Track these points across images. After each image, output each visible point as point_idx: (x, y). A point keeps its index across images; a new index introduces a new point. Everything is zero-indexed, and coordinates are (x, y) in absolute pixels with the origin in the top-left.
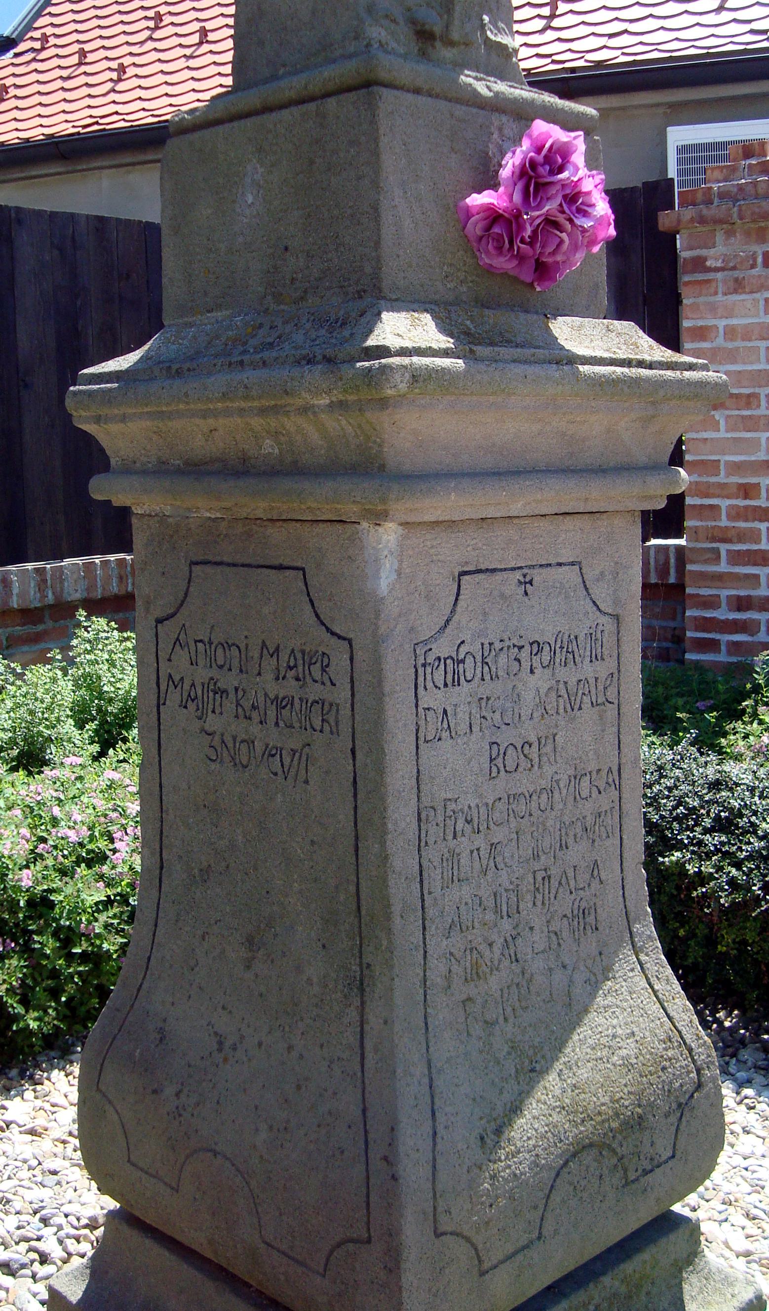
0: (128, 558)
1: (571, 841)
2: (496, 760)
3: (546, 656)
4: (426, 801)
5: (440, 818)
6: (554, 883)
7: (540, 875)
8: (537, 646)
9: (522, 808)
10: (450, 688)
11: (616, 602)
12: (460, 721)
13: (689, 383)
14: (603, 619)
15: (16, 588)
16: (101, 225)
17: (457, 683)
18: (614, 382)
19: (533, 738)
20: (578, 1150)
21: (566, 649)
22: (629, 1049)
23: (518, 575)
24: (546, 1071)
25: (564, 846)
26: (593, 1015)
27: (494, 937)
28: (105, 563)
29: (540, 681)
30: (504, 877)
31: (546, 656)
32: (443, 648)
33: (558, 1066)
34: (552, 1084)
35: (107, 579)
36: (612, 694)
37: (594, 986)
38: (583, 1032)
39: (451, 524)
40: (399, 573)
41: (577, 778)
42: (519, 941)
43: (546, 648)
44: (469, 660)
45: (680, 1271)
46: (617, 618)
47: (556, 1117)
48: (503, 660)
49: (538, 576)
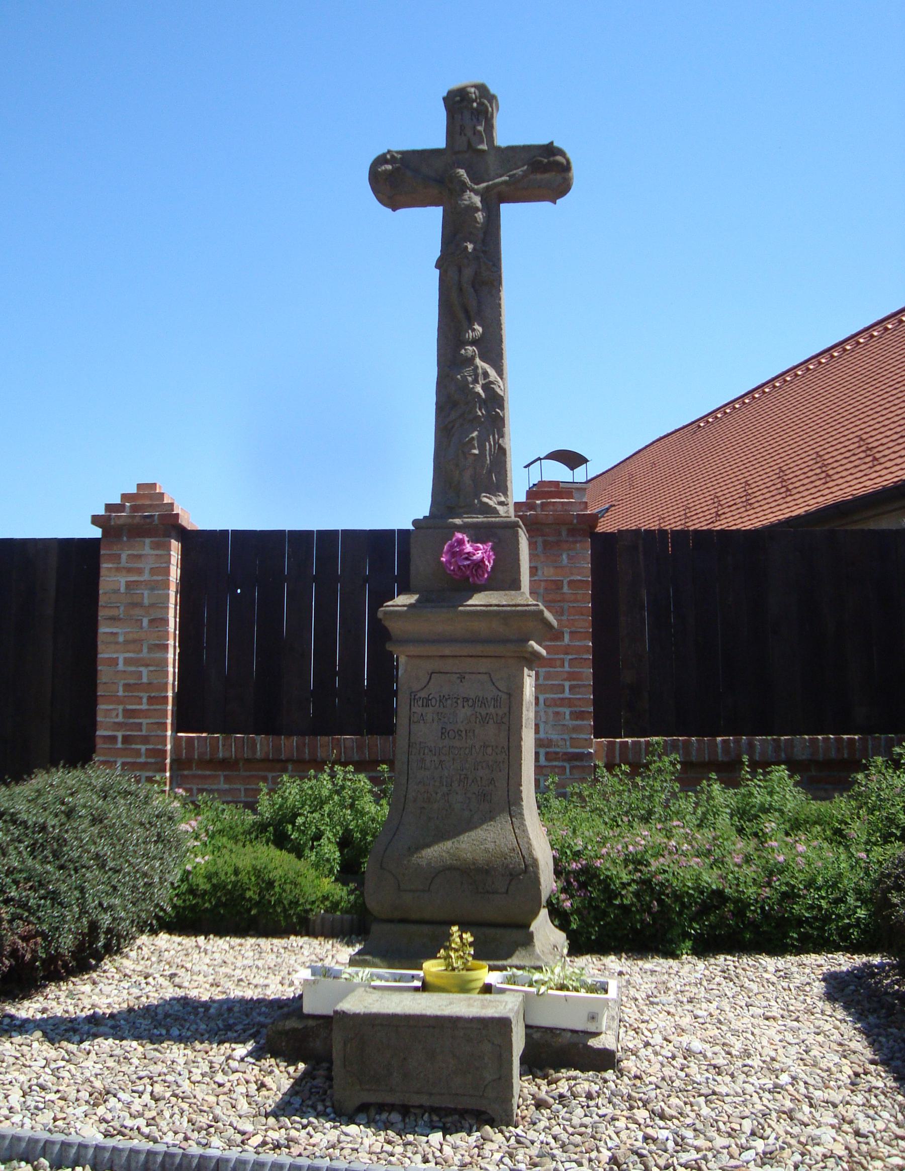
0: (856, 737)
1: (480, 767)
2: (444, 733)
3: (470, 703)
4: (412, 740)
6: (470, 781)
8: (466, 699)
13: (518, 611)
14: (500, 694)
17: (428, 706)
18: (482, 611)
19: (462, 729)
20: (451, 868)
21: (484, 703)
22: (490, 846)
23: (458, 675)
24: (448, 839)
25: (476, 769)
26: (479, 830)
28: (826, 740)
30: (446, 773)
31: (470, 703)
32: (423, 694)
33: (455, 840)
34: (449, 844)
37: (483, 821)
38: (473, 834)
39: (428, 657)
41: (485, 746)
44: (434, 700)
46: (509, 695)
47: (444, 854)
48: (449, 702)
49: (467, 676)
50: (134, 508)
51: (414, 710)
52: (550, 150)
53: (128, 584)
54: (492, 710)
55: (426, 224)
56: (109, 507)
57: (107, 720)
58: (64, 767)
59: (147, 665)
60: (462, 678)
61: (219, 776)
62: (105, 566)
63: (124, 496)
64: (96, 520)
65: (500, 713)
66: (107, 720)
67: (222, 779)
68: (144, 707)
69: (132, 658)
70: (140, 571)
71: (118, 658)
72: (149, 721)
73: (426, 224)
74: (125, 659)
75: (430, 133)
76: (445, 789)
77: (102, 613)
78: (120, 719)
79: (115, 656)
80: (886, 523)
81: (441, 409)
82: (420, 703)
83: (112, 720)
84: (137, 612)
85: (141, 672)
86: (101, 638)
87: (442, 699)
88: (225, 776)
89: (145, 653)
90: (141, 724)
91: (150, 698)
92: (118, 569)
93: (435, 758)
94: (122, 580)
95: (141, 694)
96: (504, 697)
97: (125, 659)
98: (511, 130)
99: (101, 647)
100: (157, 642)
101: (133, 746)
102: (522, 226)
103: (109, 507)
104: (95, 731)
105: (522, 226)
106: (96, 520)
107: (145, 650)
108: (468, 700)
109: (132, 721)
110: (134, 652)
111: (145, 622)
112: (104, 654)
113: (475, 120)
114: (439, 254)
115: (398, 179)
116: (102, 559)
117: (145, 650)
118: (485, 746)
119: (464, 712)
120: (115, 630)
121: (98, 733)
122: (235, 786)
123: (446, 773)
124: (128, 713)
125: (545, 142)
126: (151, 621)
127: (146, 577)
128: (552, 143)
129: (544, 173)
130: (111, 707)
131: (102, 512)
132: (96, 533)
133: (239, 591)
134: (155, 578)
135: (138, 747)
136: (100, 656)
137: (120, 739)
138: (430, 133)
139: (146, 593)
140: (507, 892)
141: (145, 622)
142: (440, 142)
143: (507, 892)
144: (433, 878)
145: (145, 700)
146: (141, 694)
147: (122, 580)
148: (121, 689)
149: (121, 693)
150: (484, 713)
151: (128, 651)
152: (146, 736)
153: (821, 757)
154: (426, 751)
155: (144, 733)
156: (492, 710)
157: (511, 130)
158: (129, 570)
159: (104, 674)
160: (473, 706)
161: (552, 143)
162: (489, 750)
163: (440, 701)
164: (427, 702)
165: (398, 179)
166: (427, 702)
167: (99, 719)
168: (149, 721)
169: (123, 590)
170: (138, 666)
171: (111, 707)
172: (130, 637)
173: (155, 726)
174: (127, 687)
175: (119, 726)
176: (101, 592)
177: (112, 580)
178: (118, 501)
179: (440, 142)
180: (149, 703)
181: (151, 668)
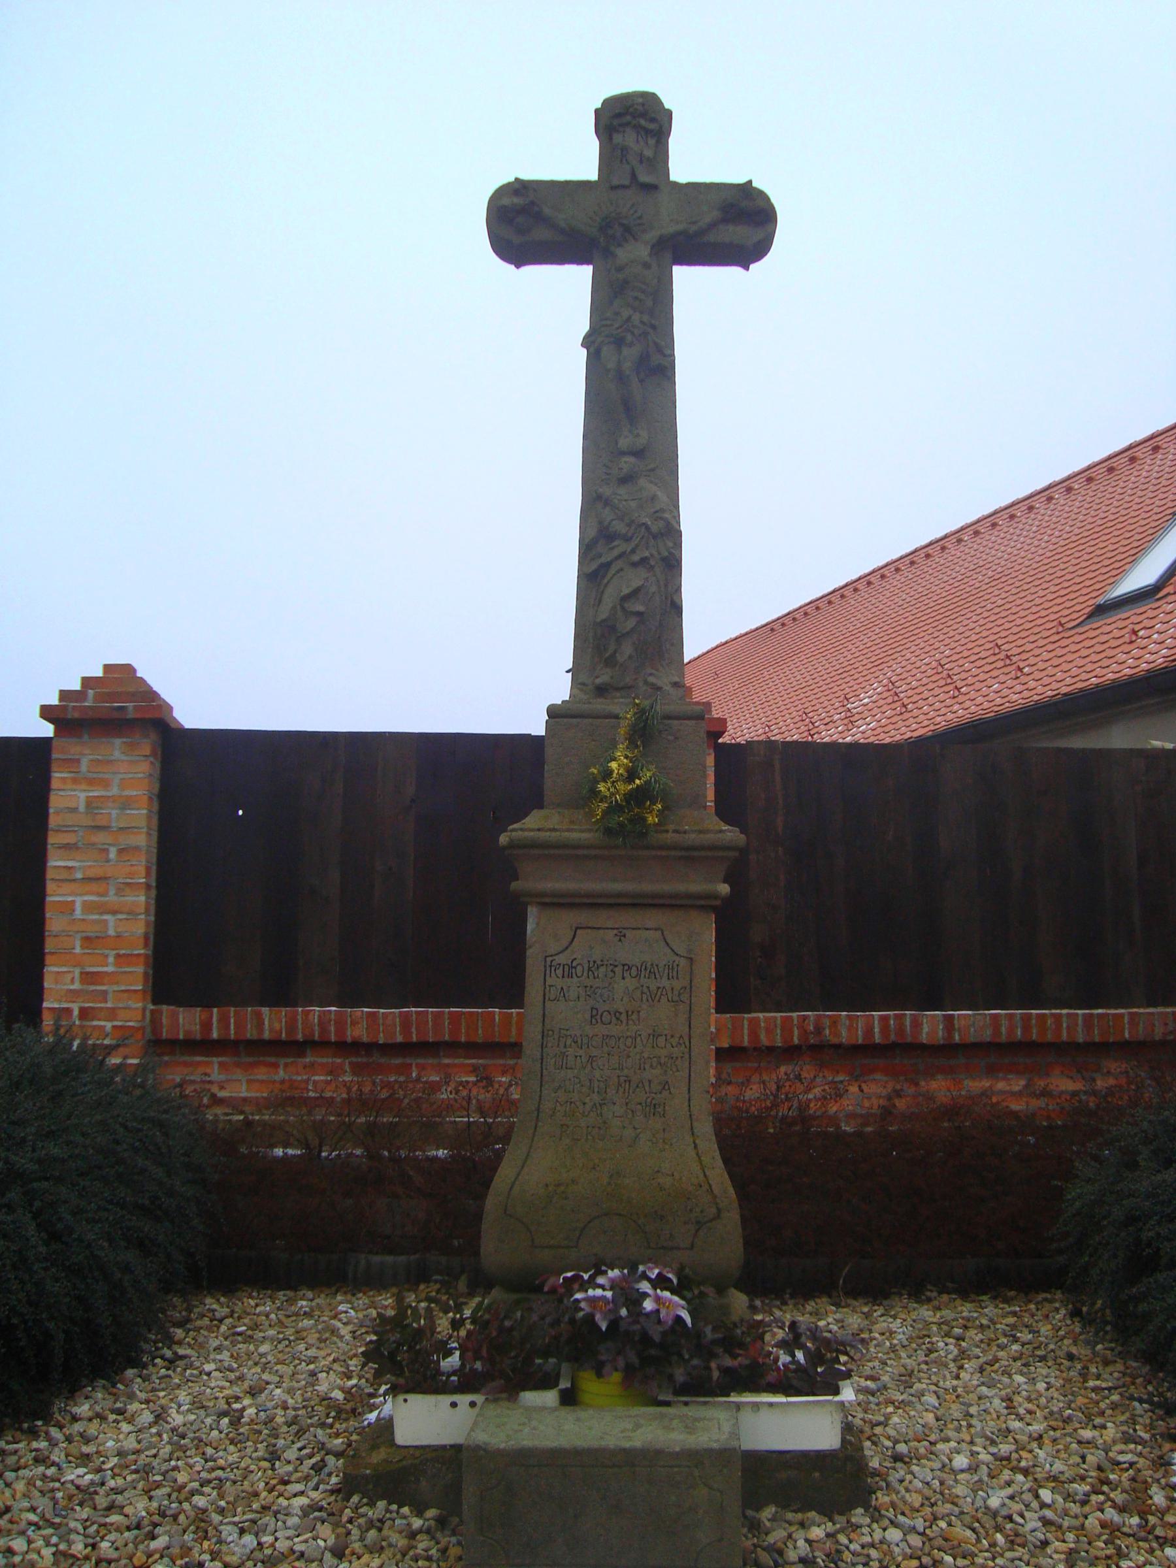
1: (647, 1067)
2: (595, 1016)
3: (634, 972)
5: (556, 1037)
7: (622, 1079)
9: (612, 1042)
10: (566, 979)
11: (690, 951)
12: (573, 994)
14: (677, 959)
15: (926, 1029)
16: (1083, 750)
17: (570, 976)
21: (651, 971)
23: (615, 931)
27: (587, 1100)
28: (1026, 1019)
29: (630, 983)
31: (634, 972)
32: (562, 959)
35: (1011, 1030)
36: (685, 997)
40: (538, 924)
41: (655, 1035)
42: (605, 1108)
43: (634, 969)
44: (579, 968)
45: (1061, 1288)
48: (602, 969)
49: (628, 933)
50: (98, 697)
51: (549, 981)
52: (747, 190)
53: (89, 803)
54: (665, 982)
55: (564, 293)
56: (64, 695)
57: (59, 987)
58: (792, 1297)
59: (114, 913)
60: (621, 937)
61: (212, 1063)
62: (58, 776)
63: (86, 681)
64: (47, 712)
65: (677, 985)
66: (59, 987)
67: (216, 1066)
68: (110, 969)
69: (92, 902)
70: (106, 784)
71: (74, 901)
72: (116, 988)
73: (564, 293)
74: (84, 903)
75: (577, 158)
76: (596, 1098)
77: (53, 839)
78: (77, 986)
79: (70, 899)
80: (1120, 737)
81: (587, 550)
82: (559, 972)
83: (66, 987)
84: (101, 838)
85: (106, 921)
86: (50, 874)
87: (593, 967)
88: (220, 1064)
89: (112, 898)
90: (105, 992)
91: (118, 956)
92: (75, 781)
93: (581, 1052)
94: (81, 796)
95: (107, 952)
96: (683, 962)
97: (84, 903)
98: (691, 160)
99: (50, 887)
100: (129, 881)
101: (95, 1023)
102: (700, 295)
103: (64, 695)
104: (42, 1001)
105: (700, 295)
106: (47, 712)
107: (112, 892)
108: (630, 968)
109: (92, 988)
110: (99, 894)
111: (113, 854)
112: (55, 895)
113: (642, 143)
114: (587, 328)
115: (527, 224)
116: (54, 767)
117: (112, 892)
118: (655, 1035)
119: (623, 985)
120: (70, 864)
121: (45, 1005)
122: (234, 1077)
123: (597, 1074)
124: (89, 978)
125: (741, 180)
126: (121, 851)
127: (114, 791)
128: (750, 182)
129: (737, 225)
130: (64, 969)
131: (54, 700)
132: (47, 730)
133: (241, 812)
134: (127, 793)
135: (102, 1023)
136: (48, 899)
137: (76, 1013)
138: (577, 158)
139: (114, 812)
140: (692, 1247)
141: (113, 854)
142: (592, 174)
143: (692, 1247)
144: (584, 1228)
145: (111, 960)
146: (107, 952)
147: (81, 796)
148: (78, 944)
149: (78, 950)
150: (653, 987)
151: (87, 894)
152: (113, 1009)
153: (1003, 1039)
154: (568, 1043)
155: (109, 1005)
156: (665, 982)
157: (691, 160)
158: (91, 782)
159: (54, 923)
160: (638, 976)
161: (750, 182)
162: (661, 1040)
163: (589, 969)
164: (570, 970)
165: (527, 224)
166: (570, 970)
167: (46, 985)
168: (116, 988)
169: (82, 808)
170: (101, 914)
171: (64, 969)
172: (91, 873)
173: (126, 995)
174: (88, 940)
175: (74, 995)
176: (51, 811)
177: (67, 797)
178: (77, 686)
179: (592, 174)
180: (117, 964)
181: (120, 916)
